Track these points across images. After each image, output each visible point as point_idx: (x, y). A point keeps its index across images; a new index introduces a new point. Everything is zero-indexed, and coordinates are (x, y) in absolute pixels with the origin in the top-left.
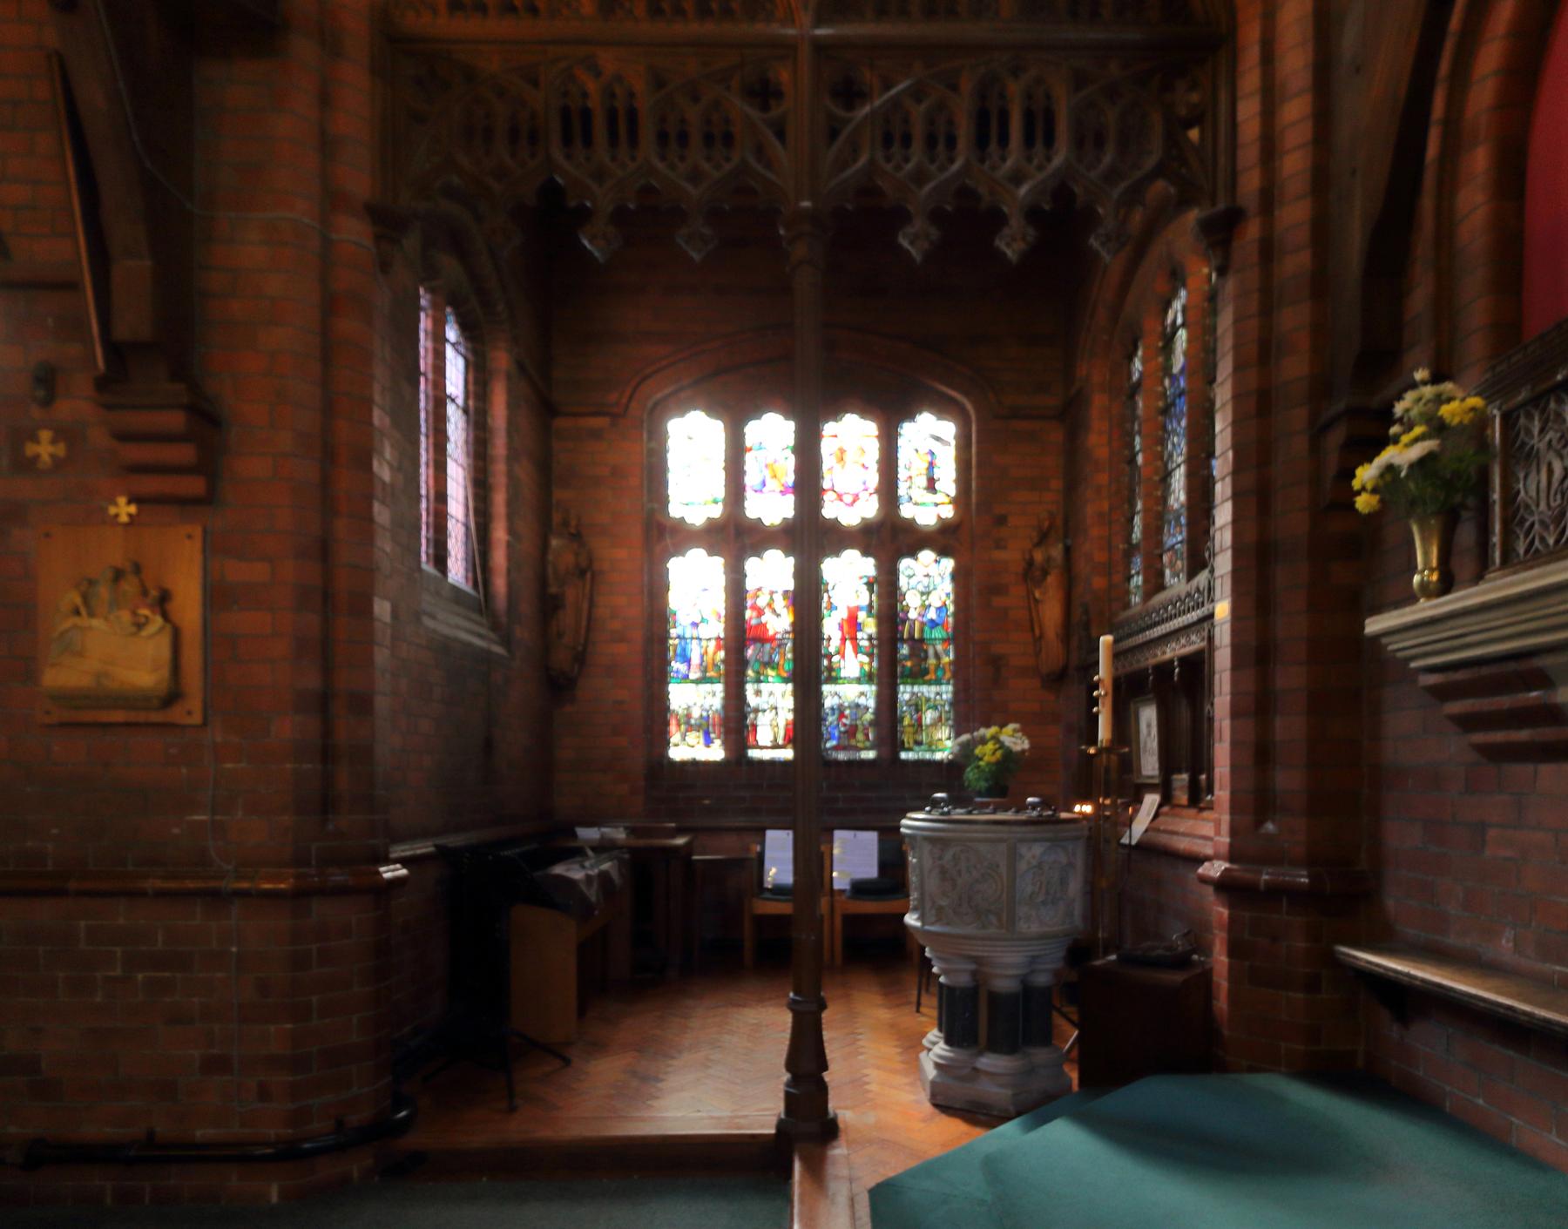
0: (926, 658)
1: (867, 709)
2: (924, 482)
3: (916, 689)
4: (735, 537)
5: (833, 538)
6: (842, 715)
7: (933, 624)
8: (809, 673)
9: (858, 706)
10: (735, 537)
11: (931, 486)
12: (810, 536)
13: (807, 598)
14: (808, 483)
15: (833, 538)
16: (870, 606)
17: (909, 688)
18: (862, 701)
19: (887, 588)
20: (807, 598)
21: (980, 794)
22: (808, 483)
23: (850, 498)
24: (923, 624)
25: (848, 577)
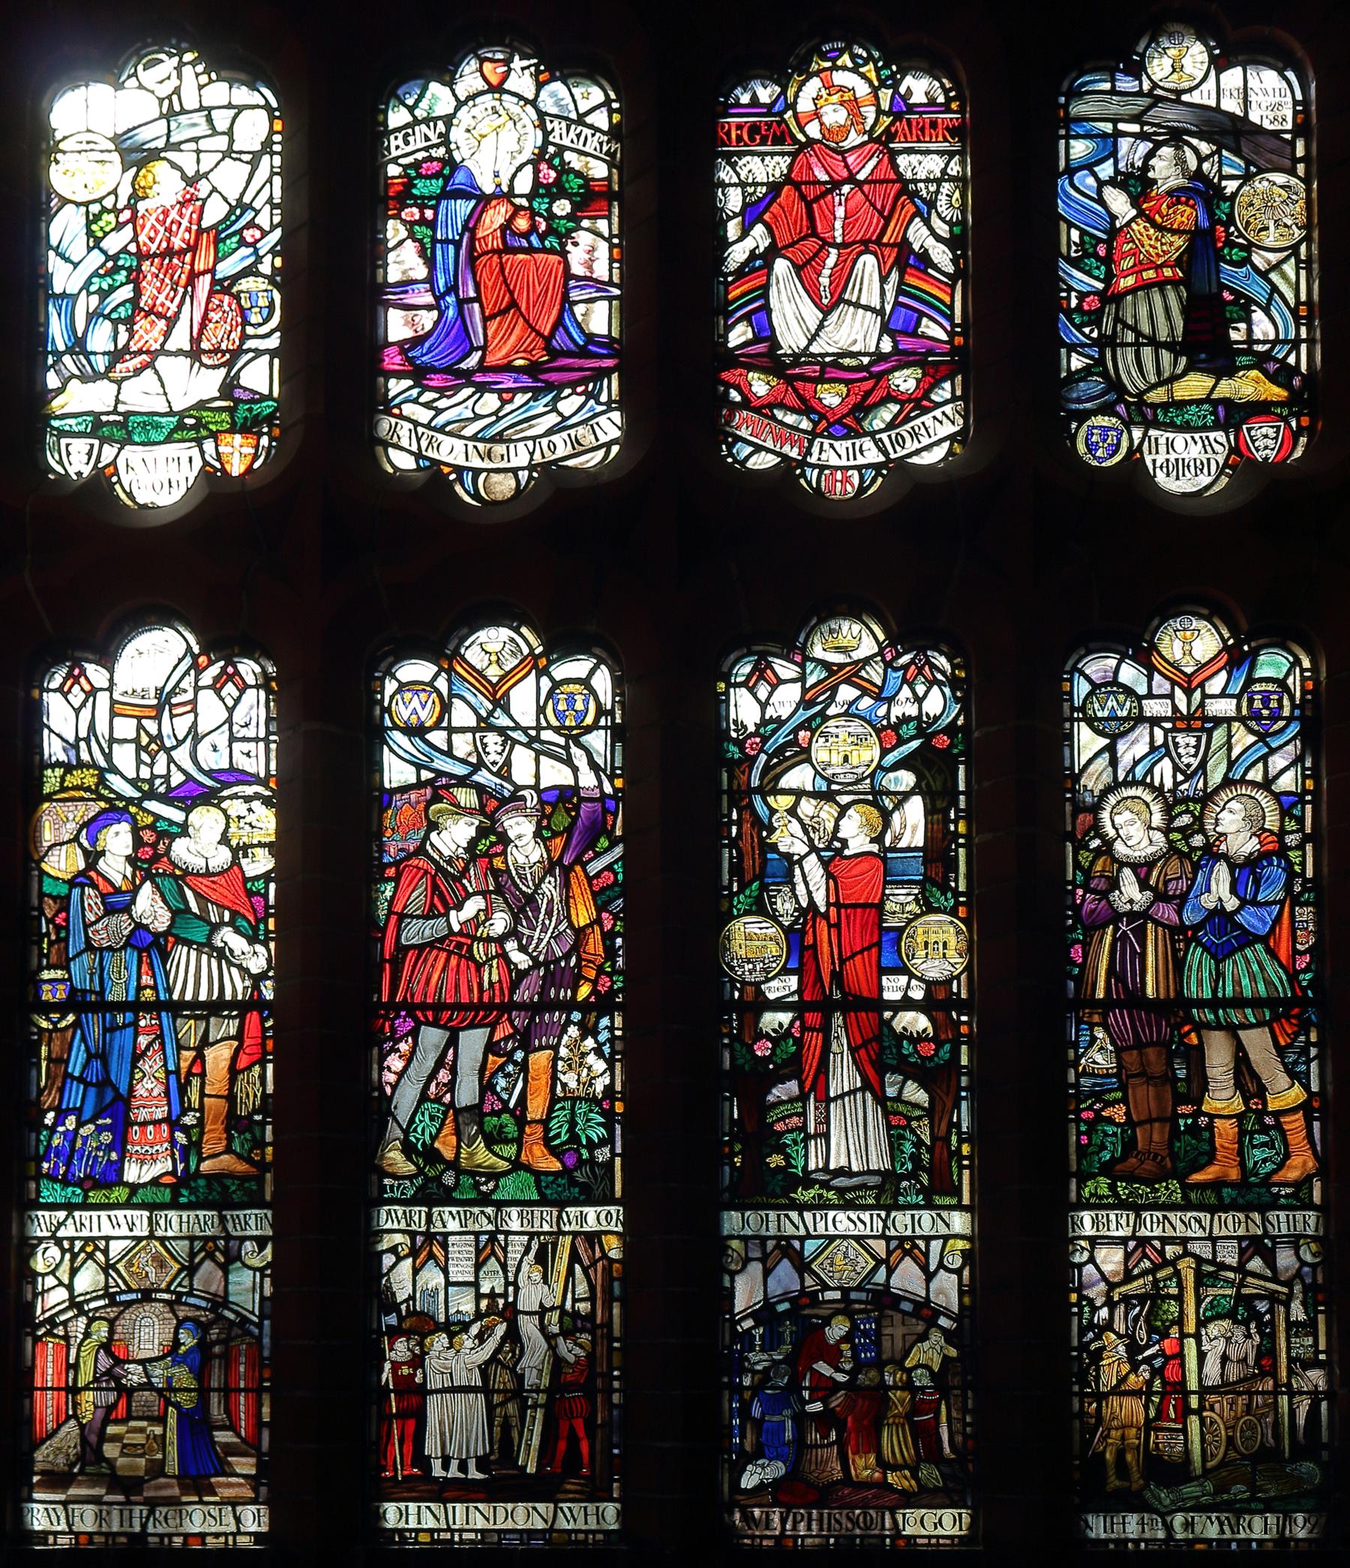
0: (1200, 1083)
1: (926, 1311)
2: (1162, 314)
3: (1152, 1226)
4: (323, 566)
5: (906, 562)
6: (810, 1343)
7: (1224, 934)
8: (695, 1127)
9: (885, 1300)
10: (323, 566)
12: (671, 563)
13: (679, 817)
14: (678, 335)
15: (906, 562)
16: (937, 851)
17: (1119, 1224)
19: (1007, 803)
20: (679, 817)
21: (784, 92)
22: (678, 335)
23: (842, 341)
25: (838, 737)
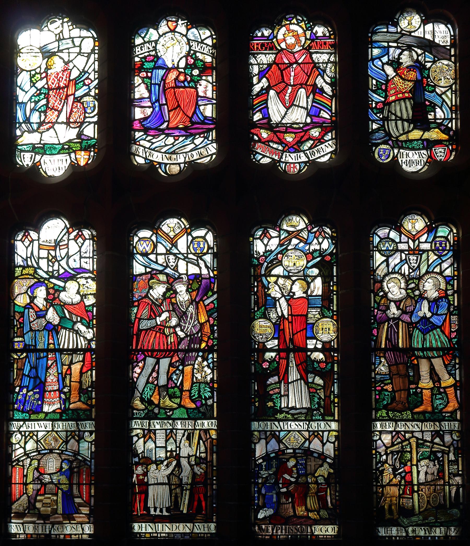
0: (418, 377)
1: (322, 457)
3: (401, 427)
4: (113, 197)
5: (315, 196)
6: (282, 468)
7: (426, 325)
8: (242, 392)
9: (308, 453)
10: (113, 197)
11: (420, 119)
12: (233, 196)
13: (237, 285)
14: (236, 117)
15: (315, 196)
16: (326, 296)
17: (390, 426)
18: (316, 445)
19: (350, 280)
22: (236, 117)
24: (411, 325)
25: (292, 256)
